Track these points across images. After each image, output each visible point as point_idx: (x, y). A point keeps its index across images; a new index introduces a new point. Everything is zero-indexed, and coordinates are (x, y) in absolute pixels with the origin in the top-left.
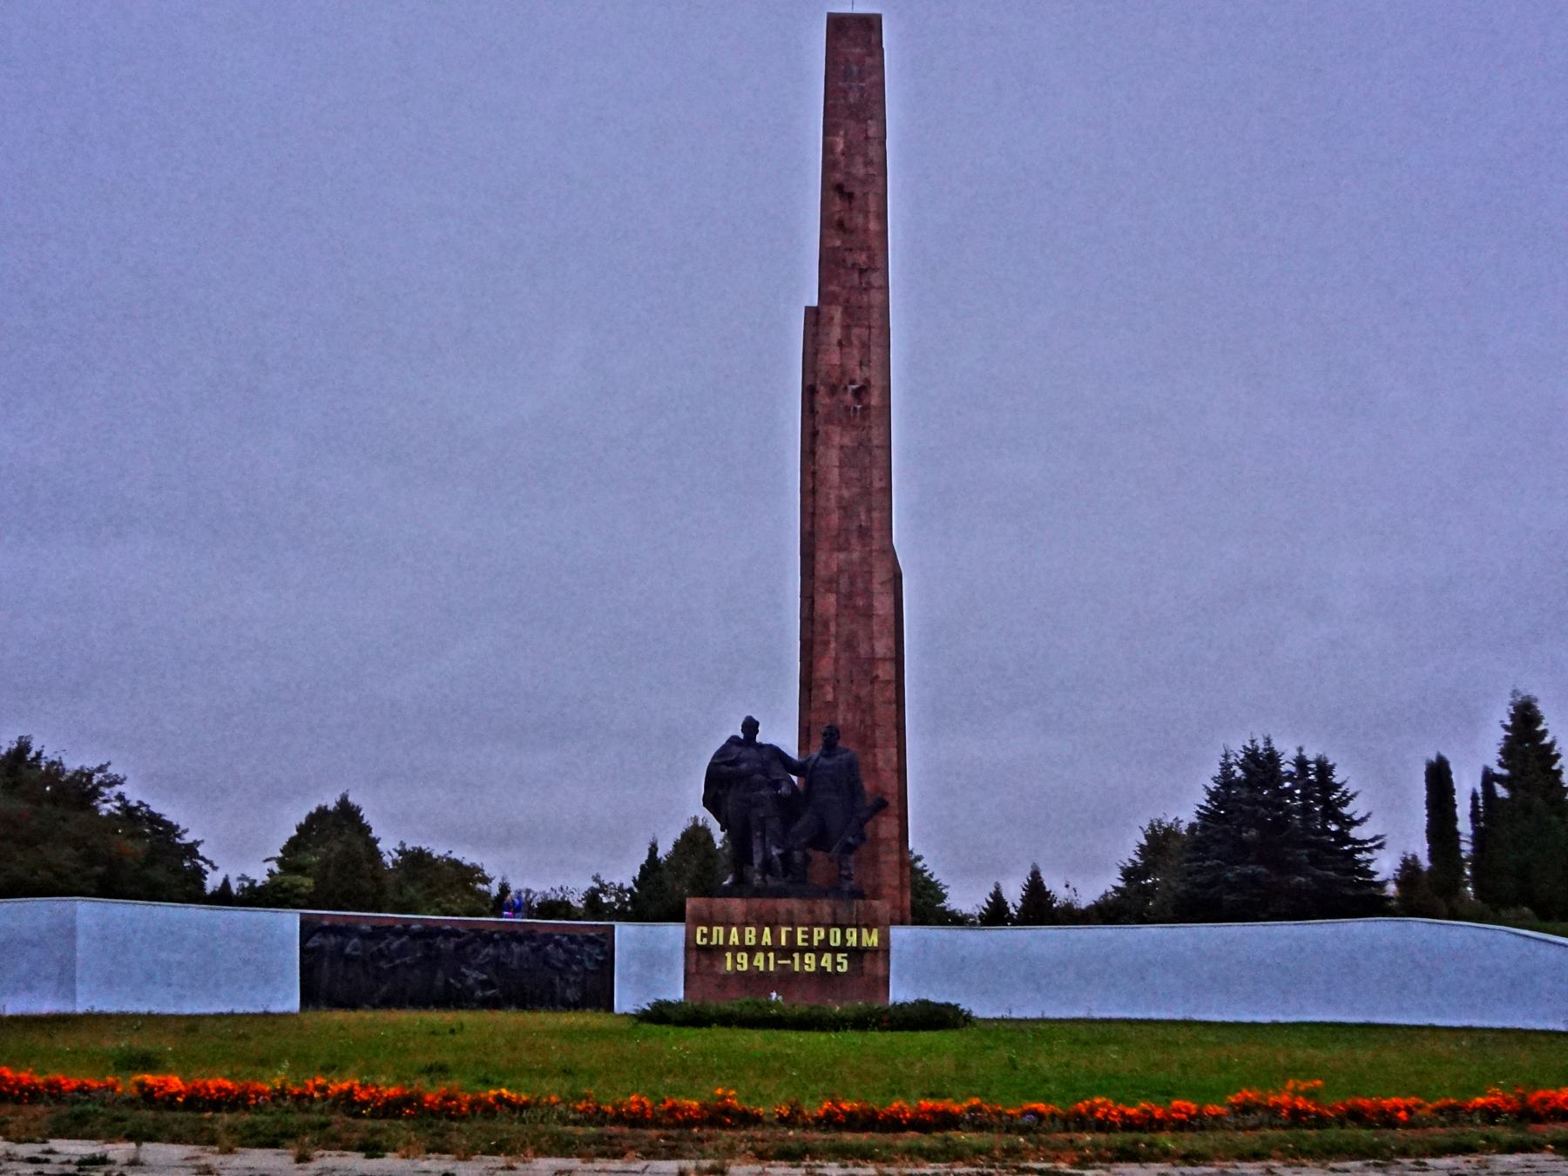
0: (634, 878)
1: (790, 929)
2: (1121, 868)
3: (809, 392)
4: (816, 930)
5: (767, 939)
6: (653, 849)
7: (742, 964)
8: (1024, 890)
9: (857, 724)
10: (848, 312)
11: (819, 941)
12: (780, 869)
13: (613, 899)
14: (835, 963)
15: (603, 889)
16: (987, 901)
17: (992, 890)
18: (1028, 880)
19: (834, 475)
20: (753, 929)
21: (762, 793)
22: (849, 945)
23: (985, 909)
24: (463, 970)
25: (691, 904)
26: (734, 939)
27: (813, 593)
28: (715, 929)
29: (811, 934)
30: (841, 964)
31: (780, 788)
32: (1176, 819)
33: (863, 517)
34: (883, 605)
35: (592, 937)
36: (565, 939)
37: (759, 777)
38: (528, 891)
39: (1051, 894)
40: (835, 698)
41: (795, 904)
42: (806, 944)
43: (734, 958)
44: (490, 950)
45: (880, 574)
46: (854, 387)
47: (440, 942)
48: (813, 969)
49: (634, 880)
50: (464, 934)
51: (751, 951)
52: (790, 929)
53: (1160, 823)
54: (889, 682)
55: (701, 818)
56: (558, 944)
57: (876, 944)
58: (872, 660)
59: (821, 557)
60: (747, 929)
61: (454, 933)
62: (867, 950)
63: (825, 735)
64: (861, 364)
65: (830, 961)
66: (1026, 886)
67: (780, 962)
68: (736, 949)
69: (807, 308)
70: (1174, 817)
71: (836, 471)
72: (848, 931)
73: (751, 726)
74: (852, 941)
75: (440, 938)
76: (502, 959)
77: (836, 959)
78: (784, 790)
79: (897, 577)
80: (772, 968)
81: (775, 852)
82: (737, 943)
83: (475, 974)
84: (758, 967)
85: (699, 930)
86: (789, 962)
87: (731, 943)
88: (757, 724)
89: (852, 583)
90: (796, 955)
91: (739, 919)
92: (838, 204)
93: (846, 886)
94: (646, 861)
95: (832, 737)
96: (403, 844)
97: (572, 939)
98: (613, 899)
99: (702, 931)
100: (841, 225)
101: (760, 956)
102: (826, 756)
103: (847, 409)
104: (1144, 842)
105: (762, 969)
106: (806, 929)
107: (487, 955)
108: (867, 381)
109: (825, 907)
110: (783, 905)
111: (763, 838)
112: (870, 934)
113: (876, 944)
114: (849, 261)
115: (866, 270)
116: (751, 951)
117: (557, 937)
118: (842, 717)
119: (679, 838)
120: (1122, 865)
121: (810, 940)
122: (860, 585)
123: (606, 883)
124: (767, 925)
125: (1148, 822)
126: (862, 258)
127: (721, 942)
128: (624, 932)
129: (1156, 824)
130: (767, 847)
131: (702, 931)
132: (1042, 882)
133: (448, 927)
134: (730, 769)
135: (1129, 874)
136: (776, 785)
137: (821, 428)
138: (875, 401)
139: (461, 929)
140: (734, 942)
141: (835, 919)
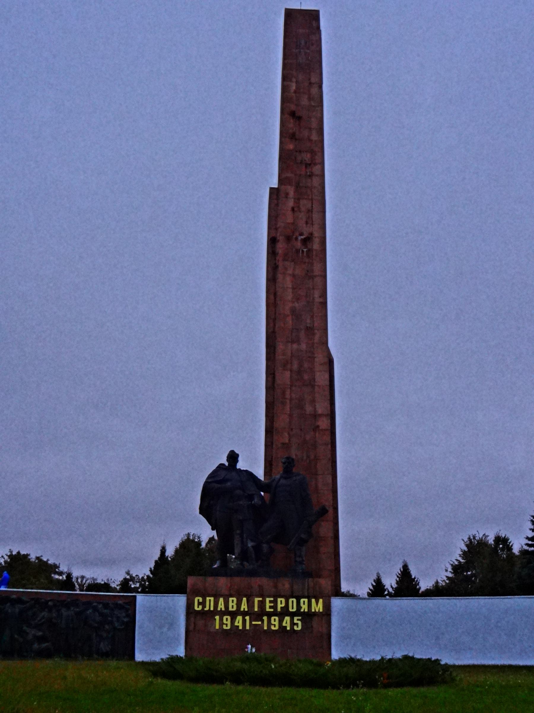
0: (151, 568)
1: (261, 599)
2: (452, 565)
3: (272, 241)
4: (279, 600)
5: (244, 607)
6: (163, 551)
7: (227, 625)
8: (398, 577)
9: (305, 458)
10: (298, 187)
11: (281, 608)
12: (253, 556)
13: (138, 585)
14: (293, 624)
15: (132, 579)
16: (372, 585)
17: (375, 577)
18: (401, 571)
19: (289, 296)
20: (235, 599)
21: (241, 503)
22: (302, 610)
23: (370, 590)
24: (25, 628)
25: (191, 581)
26: (221, 606)
27: (274, 371)
28: (208, 599)
29: (275, 602)
30: (297, 624)
31: (253, 499)
32: (484, 534)
33: (308, 321)
34: (321, 378)
35: (120, 604)
36: (100, 606)
37: (238, 492)
38: (83, 577)
39: (416, 580)
40: (289, 440)
41: (265, 582)
42: (272, 610)
43: (221, 620)
44: (45, 614)
45: (320, 358)
46: (302, 237)
48: (229, 627)
49: (151, 570)
50: (27, 602)
51: (233, 615)
52: (261, 599)
53: (474, 537)
54: (327, 430)
55: (192, 534)
56: (95, 609)
57: (321, 610)
58: (315, 416)
59: (280, 347)
60: (231, 599)
61: (19, 600)
62: (315, 614)
63: (284, 463)
64: (307, 223)
65: (289, 622)
66: (399, 574)
67: (253, 623)
68: (222, 614)
69: (271, 189)
70: (483, 534)
71: (290, 291)
72: (302, 600)
73: (233, 457)
74: (304, 608)
75: (8, 604)
76: (54, 620)
77: (293, 620)
78: (256, 500)
79: (330, 362)
80: (248, 627)
81: (250, 544)
82: (223, 609)
83: (33, 632)
84: (238, 626)
85: (196, 599)
86: (260, 623)
87: (219, 609)
88: (238, 455)
89: (301, 366)
90: (265, 618)
91: (225, 591)
92: (291, 124)
93: (299, 569)
94: (159, 558)
95: (289, 464)
96: (11, 551)
97: (106, 606)
98: (138, 585)
99: (198, 600)
100: (293, 137)
101: (239, 618)
102: (285, 478)
103: (297, 251)
104: (466, 549)
105: (241, 628)
106: (272, 599)
107: (43, 617)
108: (311, 234)
109: (285, 584)
110: (256, 582)
111: (241, 535)
112: (317, 603)
113: (321, 610)
114: (299, 158)
115: (310, 164)
116: (233, 615)
117: (95, 604)
118: (294, 453)
119: (178, 546)
120: (452, 563)
121: (275, 607)
122: (306, 365)
123: (134, 575)
124: (245, 596)
125: (468, 537)
126: (307, 157)
127: (212, 609)
128: (140, 598)
129: (472, 538)
130: (245, 540)
131: (198, 600)
132: (410, 572)
133: (14, 596)
134: (219, 486)
135: (456, 569)
136: (251, 497)
137: (280, 264)
138: (316, 246)
139: (24, 598)
140: (221, 608)
141: (292, 592)
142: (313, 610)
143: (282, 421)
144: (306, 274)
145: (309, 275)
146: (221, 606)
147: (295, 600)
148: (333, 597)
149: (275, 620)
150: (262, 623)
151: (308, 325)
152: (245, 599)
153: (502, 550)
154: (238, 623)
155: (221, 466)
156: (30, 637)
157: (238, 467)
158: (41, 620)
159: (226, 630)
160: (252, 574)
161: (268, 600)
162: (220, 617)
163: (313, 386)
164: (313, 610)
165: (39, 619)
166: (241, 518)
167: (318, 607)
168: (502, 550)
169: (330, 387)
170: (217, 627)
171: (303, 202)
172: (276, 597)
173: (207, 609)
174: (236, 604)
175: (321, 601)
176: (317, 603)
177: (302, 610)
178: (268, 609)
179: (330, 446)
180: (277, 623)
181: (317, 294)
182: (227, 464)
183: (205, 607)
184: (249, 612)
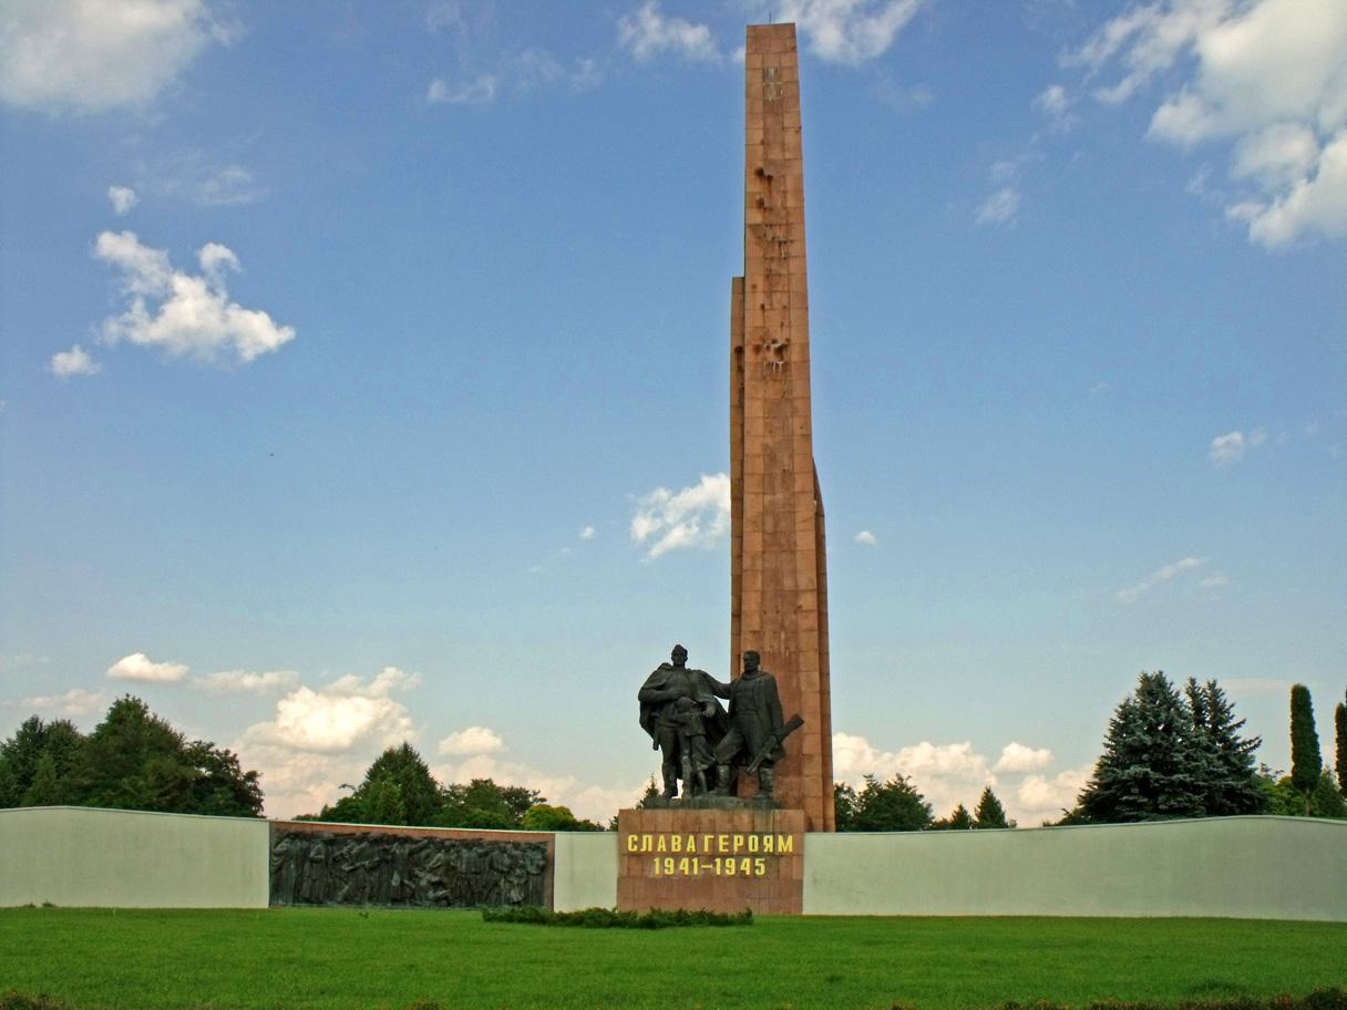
4: (736, 837)
5: (691, 847)
14: (754, 867)
20: (679, 837)
22: (766, 850)
26: (662, 847)
29: (731, 840)
30: (759, 868)
33: (786, 461)
37: (684, 699)
40: (762, 628)
43: (662, 863)
46: (777, 346)
47: (395, 848)
51: (677, 857)
54: (812, 611)
56: (504, 851)
57: (791, 850)
60: (674, 837)
61: (406, 840)
65: (748, 865)
68: (663, 856)
72: (765, 838)
73: (680, 654)
74: (769, 847)
75: (396, 844)
76: (452, 864)
80: (696, 871)
82: (664, 850)
85: (630, 837)
86: (711, 866)
87: (659, 850)
89: (776, 524)
101: (685, 861)
106: (727, 836)
107: (439, 860)
111: (692, 760)
112: (785, 840)
113: (791, 850)
116: (677, 857)
121: (730, 846)
124: (693, 833)
126: (780, 234)
127: (650, 849)
136: (702, 706)
141: (753, 827)
142: (780, 850)
143: (751, 603)
144: (783, 397)
145: (786, 397)
146: (662, 847)
147: (756, 838)
149: (731, 863)
151: (786, 468)
152: (691, 838)
153: (517, 798)
155: (664, 667)
156: (423, 883)
157: (687, 667)
160: (703, 805)
161: (721, 837)
163: (793, 552)
164: (780, 850)
166: (688, 734)
168: (517, 798)
169: (817, 554)
170: (657, 872)
171: (776, 297)
175: (790, 838)
176: (785, 840)
177: (766, 850)
178: (721, 849)
179: (816, 633)
180: (733, 867)
181: (797, 422)
182: (672, 663)
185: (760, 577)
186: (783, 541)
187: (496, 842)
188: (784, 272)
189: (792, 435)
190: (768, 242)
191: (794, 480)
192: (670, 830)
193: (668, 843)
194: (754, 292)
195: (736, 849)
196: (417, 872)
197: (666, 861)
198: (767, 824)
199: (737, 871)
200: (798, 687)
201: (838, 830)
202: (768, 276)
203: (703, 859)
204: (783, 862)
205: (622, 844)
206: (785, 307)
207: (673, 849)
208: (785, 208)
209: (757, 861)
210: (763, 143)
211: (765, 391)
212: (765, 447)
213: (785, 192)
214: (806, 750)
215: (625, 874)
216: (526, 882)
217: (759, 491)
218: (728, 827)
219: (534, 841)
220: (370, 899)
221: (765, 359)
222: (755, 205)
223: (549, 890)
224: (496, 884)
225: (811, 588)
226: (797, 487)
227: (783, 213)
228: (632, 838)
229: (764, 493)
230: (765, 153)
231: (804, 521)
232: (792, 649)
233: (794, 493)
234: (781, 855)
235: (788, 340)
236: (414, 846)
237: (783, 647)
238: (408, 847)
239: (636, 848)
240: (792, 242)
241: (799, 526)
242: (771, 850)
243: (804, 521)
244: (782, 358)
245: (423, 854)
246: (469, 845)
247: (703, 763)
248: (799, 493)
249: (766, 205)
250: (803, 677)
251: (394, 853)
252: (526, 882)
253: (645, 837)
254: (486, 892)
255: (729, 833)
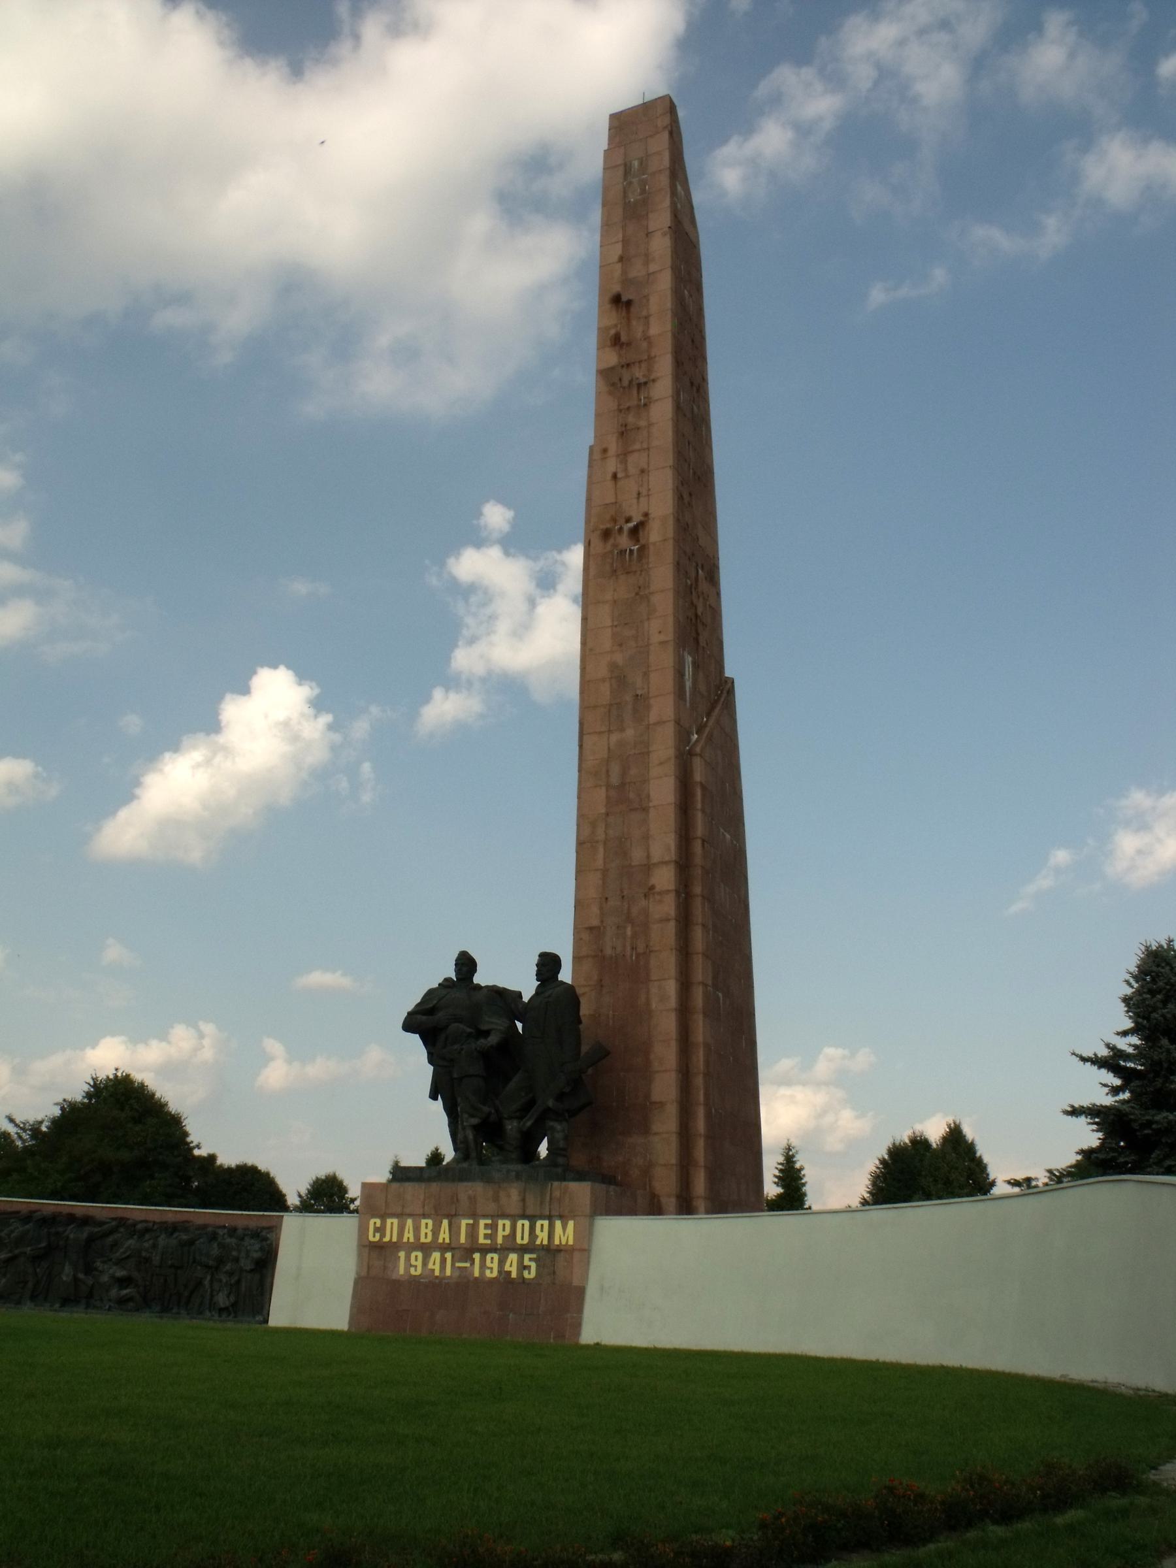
1: (471, 1222)
4: (501, 1222)
5: (444, 1236)
14: (522, 1267)
20: (430, 1222)
22: (538, 1242)
26: (409, 1236)
29: (493, 1227)
30: (528, 1268)
40: (602, 922)
42: (489, 1242)
43: (408, 1258)
46: (631, 525)
51: (426, 1249)
52: (471, 1222)
54: (668, 891)
57: (571, 1242)
60: (424, 1222)
61: (86, 1221)
67: (458, 1265)
72: (539, 1223)
73: (466, 964)
74: (542, 1237)
80: (448, 1272)
82: (412, 1240)
86: (467, 1265)
87: (405, 1240)
89: (624, 772)
90: (477, 1256)
101: (436, 1255)
106: (489, 1221)
112: (564, 1227)
113: (571, 1242)
116: (426, 1249)
126: (639, 373)
127: (395, 1239)
142: (557, 1242)
144: (637, 594)
146: (409, 1236)
148: (599, 1217)
149: (493, 1260)
150: (471, 1265)
151: (639, 692)
152: (445, 1223)
154: (434, 1264)
156: (105, 1278)
158: (124, 1253)
159: (415, 1276)
161: (482, 1222)
162: (406, 1254)
163: (645, 810)
164: (557, 1242)
165: (121, 1250)
167: (566, 1235)
170: (402, 1271)
171: (632, 459)
172: (532, 1219)
173: (387, 1239)
174: (432, 1231)
175: (571, 1224)
176: (564, 1227)
177: (538, 1242)
178: (482, 1240)
180: (495, 1266)
183: (385, 1236)
184: (453, 1246)
185: (601, 850)
186: (632, 795)
187: (205, 1227)
188: (643, 423)
189: (648, 645)
190: (624, 388)
191: (648, 707)
192: (421, 1212)
193: (417, 1230)
194: (604, 459)
195: (500, 1240)
196: (98, 1264)
197: (413, 1255)
198: (542, 1203)
199: (500, 1272)
200: (648, 1003)
201: (710, 1211)
202: (622, 433)
203: (458, 1254)
204: (561, 1258)
205: (363, 1230)
206: (643, 471)
207: (423, 1240)
208: (647, 338)
209: (527, 1257)
210: (621, 259)
211: (615, 590)
212: (613, 666)
213: (647, 317)
214: (656, 1096)
215: (364, 1273)
216: (238, 1282)
217: (604, 729)
218: (491, 1207)
219: (253, 1224)
220: (33, 1298)
221: (615, 546)
222: (609, 343)
223: (268, 1297)
224: (199, 1283)
225: (667, 859)
226: (653, 717)
227: (645, 345)
228: (374, 1222)
229: (610, 731)
230: (624, 272)
231: (661, 764)
232: (641, 949)
233: (648, 727)
234: (559, 1250)
235: (646, 515)
236: (96, 1230)
237: (628, 948)
238: (84, 1234)
239: (378, 1235)
240: (654, 381)
241: (655, 771)
242: (545, 1242)
243: (661, 764)
244: (637, 541)
245: (110, 1239)
246: (172, 1228)
247: (472, 1116)
248: (655, 724)
249: (624, 338)
250: (654, 990)
251: (68, 1237)
252: (238, 1282)
253: (389, 1221)
254: (186, 1294)
255: (492, 1217)
